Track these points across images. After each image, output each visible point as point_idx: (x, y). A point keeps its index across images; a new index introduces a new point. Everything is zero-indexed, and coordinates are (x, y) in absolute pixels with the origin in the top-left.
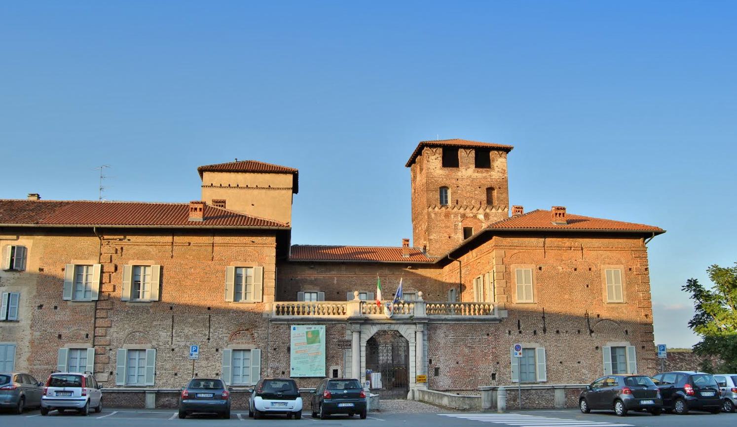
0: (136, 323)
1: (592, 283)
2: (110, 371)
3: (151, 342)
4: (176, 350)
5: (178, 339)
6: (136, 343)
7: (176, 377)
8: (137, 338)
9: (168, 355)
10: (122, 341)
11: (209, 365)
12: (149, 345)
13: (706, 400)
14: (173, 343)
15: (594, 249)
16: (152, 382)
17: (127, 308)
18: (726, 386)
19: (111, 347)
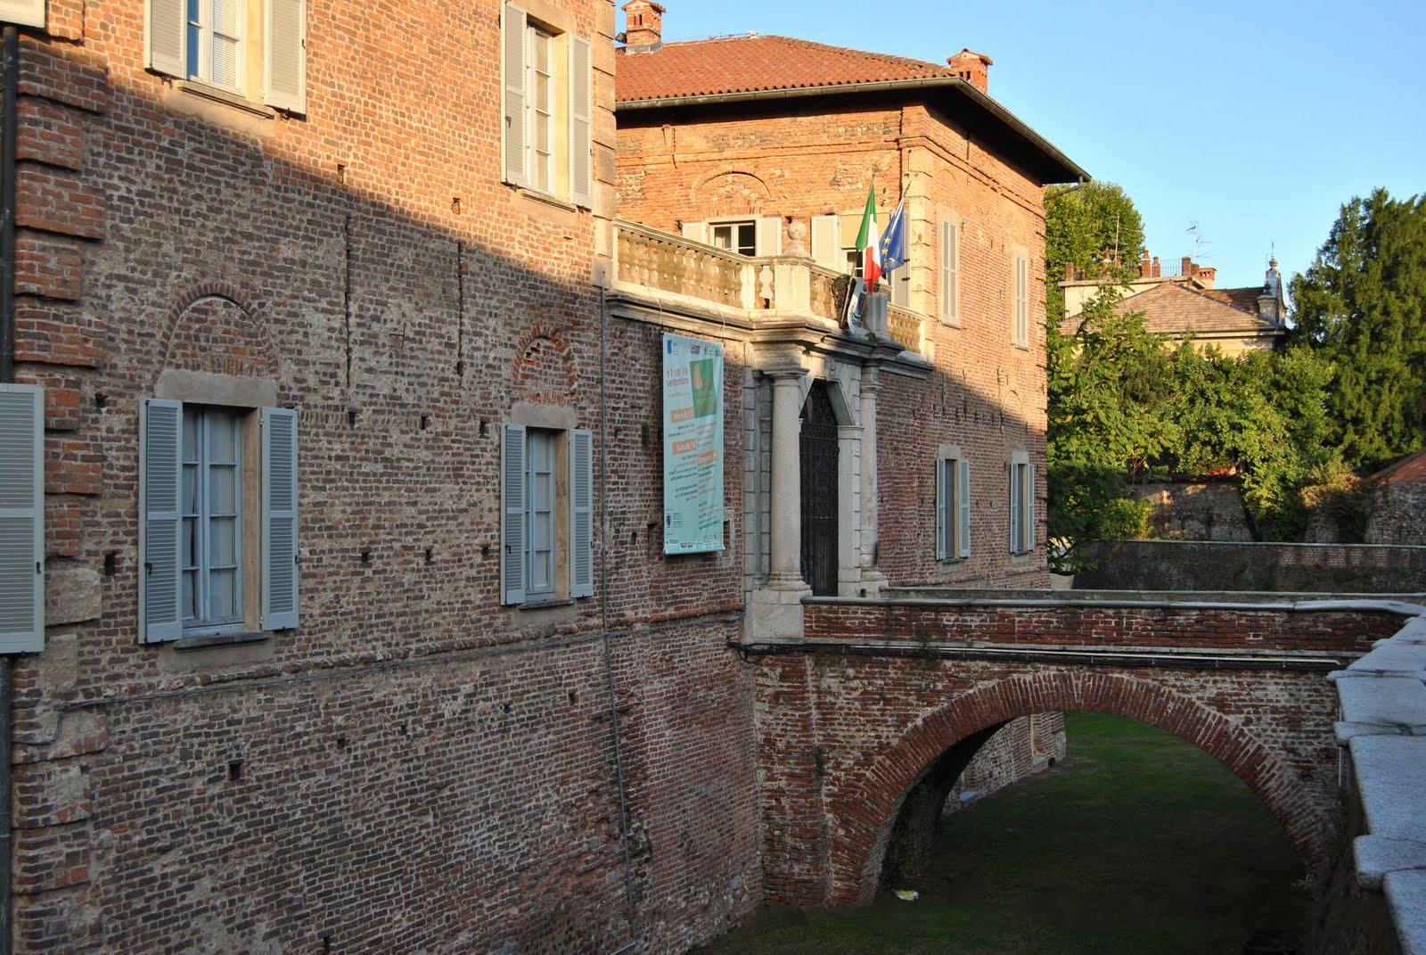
0: (210, 238)
1: (965, 547)
2: (107, 547)
3: (273, 366)
4: (365, 415)
5: (368, 352)
6: (216, 366)
7: (368, 572)
8: (218, 332)
9: (337, 448)
10: (154, 345)
11: (464, 505)
12: (269, 384)
13: (523, 527)
14: (355, 379)
15: (942, 151)
16: (28, 626)
17: (169, 124)
18: (1370, 350)
19: (108, 385)
